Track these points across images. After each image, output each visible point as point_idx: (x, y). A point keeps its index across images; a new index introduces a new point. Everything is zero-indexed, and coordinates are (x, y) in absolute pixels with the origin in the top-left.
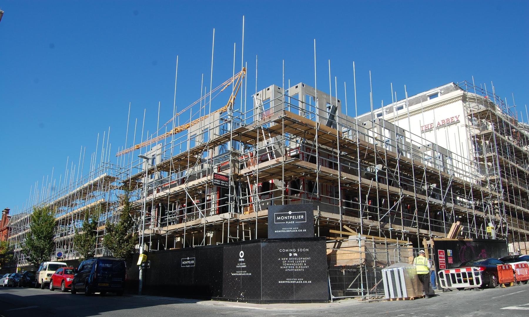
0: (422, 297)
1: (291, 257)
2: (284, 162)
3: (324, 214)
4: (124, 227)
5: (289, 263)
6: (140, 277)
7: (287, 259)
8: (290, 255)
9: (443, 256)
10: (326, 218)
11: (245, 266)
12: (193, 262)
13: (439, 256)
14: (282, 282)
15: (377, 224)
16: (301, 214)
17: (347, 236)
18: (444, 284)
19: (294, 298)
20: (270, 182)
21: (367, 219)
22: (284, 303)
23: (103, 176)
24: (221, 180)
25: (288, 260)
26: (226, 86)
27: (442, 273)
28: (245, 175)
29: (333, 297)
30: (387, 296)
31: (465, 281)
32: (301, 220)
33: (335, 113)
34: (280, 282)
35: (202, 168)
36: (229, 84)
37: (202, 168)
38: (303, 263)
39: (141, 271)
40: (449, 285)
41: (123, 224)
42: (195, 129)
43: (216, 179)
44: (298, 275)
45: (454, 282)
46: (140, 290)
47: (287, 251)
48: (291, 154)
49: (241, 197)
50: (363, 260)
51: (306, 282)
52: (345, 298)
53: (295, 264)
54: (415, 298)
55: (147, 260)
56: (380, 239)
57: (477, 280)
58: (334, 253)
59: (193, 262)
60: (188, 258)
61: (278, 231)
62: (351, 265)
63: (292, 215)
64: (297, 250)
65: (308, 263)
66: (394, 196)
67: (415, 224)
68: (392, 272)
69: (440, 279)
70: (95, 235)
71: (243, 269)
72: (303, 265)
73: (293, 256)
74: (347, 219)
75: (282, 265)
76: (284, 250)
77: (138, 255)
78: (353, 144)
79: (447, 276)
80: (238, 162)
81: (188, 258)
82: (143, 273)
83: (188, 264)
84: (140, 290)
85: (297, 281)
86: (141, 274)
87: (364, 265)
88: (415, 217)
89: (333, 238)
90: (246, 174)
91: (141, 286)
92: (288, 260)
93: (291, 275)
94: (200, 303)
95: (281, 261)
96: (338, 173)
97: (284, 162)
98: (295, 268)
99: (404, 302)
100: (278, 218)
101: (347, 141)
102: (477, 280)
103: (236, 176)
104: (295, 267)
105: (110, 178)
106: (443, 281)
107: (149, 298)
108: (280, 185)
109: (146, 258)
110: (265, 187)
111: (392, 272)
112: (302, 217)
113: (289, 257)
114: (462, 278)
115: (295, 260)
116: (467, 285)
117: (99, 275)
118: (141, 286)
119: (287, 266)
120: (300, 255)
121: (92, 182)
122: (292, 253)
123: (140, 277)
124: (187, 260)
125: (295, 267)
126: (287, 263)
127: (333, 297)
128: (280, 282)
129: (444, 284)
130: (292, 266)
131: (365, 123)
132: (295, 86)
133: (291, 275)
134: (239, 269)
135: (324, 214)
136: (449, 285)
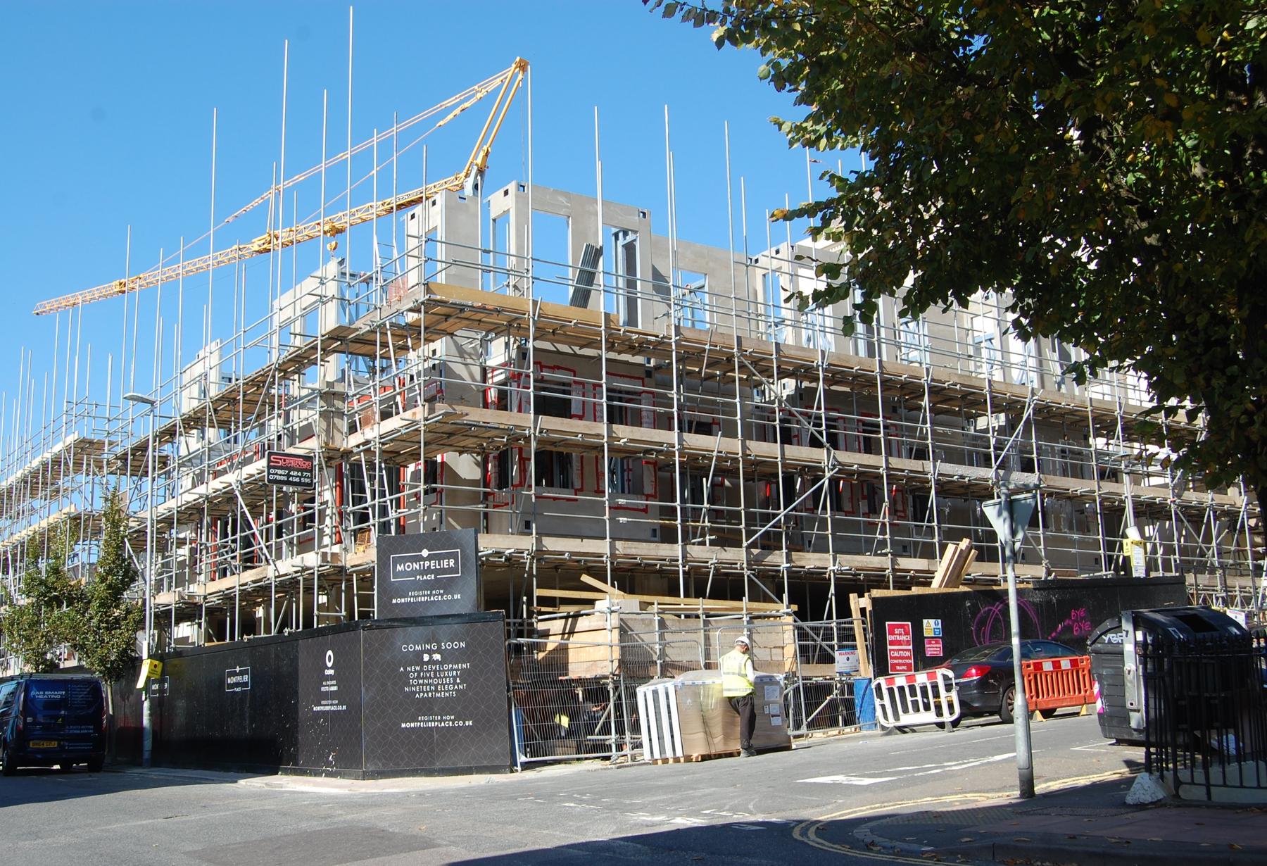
0: (730, 755)
1: (427, 663)
2: (426, 419)
3: (551, 544)
4: (109, 587)
5: (423, 678)
6: (146, 721)
7: (418, 668)
8: (426, 657)
9: (904, 638)
10: (562, 553)
11: (335, 688)
12: (246, 678)
13: (889, 638)
14: (408, 725)
15: (737, 556)
16: (449, 556)
17: (591, 602)
18: (886, 718)
19: (438, 766)
20: (439, 459)
21: (703, 543)
22: (414, 775)
23: (71, 439)
24: (290, 469)
25: (421, 670)
26: (457, 111)
27: (879, 685)
28: (355, 450)
29: (522, 758)
30: (647, 757)
31: (927, 708)
32: (450, 571)
33: (595, 265)
34: (403, 725)
35: (287, 421)
36: (467, 105)
37: (287, 421)
38: (454, 678)
39: (146, 704)
40: (897, 718)
41: (103, 580)
42: (287, 306)
43: (274, 467)
44: (445, 707)
45: (906, 711)
46: (146, 755)
47: (418, 648)
48: (496, 380)
49: (351, 508)
50: (616, 664)
51: (461, 723)
52: (578, 759)
53: (435, 681)
54: (705, 758)
55: (163, 673)
56: (682, 602)
57: (951, 706)
58: (563, 650)
59: (246, 678)
60: (238, 669)
61: (399, 601)
62: (588, 676)
63: (430, 558)
64: (440, 647)
65: (465, 676)
66: (813, 473)
67: (883, 544)
68: (655, 693)
69: (877, 702)
70: (59, 606)
71: (332, 695)
72: (455, 683)
73: (431, 662)
74: (633, 552)
75: (408, 685)
76: (411, 648)
77: (140, 660)
78: (660, 343)
79: (891, 691)
80: (341, 414)
81: (238, 669)
82: (151, 708)
83: (237, 685)
84: (146, 755)
85: (441, 721)
86: (146, 712)
87: (618, 675)
88: (884, 524)
89: (550, 609)
90: (358, 446)
91: (148, 744)
92: (421, 670)
93: (428, 706)
94: (242, 782)
95: (406, 673)
96: (603, 428)
97: (426, 419)
98: (436, 691)
99: (683, 765)
100: (400, 568)
101: (635, 337)
102: (951, 706)
103: (334, 457)
104: (436, 686)
105: (91, 443)
106: (883, 707)
107: (155, 773)
108: (466, 466)
109: (159, 669)
110: (434, 472)
111: (655, 693)
112: (452, 562)
113: (422, 663)
114: (919, 698)
115: (435, 671)
116: (931, 717)
117: (29, 720)
118: (148, 744)
119: (419, 688)
120: (448, 657)
121: (48, 455)
122: (430, 652)
123: (146, 721)
124: (235, 674)
125: (436, 686)
126: (418, 678)
127: (522, 758)
128: (403, 725)
129: (886, 718)
130: (430, 685)
131: (754, 258)
132: (502, 192)
133: (428, 706)
134: (326, 695)
135: (551, 544)
136: (897, 718)
